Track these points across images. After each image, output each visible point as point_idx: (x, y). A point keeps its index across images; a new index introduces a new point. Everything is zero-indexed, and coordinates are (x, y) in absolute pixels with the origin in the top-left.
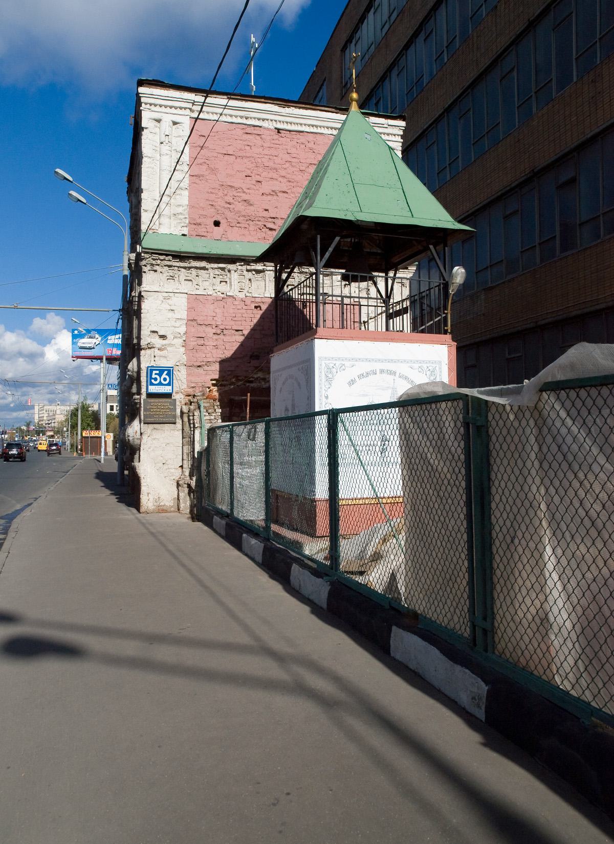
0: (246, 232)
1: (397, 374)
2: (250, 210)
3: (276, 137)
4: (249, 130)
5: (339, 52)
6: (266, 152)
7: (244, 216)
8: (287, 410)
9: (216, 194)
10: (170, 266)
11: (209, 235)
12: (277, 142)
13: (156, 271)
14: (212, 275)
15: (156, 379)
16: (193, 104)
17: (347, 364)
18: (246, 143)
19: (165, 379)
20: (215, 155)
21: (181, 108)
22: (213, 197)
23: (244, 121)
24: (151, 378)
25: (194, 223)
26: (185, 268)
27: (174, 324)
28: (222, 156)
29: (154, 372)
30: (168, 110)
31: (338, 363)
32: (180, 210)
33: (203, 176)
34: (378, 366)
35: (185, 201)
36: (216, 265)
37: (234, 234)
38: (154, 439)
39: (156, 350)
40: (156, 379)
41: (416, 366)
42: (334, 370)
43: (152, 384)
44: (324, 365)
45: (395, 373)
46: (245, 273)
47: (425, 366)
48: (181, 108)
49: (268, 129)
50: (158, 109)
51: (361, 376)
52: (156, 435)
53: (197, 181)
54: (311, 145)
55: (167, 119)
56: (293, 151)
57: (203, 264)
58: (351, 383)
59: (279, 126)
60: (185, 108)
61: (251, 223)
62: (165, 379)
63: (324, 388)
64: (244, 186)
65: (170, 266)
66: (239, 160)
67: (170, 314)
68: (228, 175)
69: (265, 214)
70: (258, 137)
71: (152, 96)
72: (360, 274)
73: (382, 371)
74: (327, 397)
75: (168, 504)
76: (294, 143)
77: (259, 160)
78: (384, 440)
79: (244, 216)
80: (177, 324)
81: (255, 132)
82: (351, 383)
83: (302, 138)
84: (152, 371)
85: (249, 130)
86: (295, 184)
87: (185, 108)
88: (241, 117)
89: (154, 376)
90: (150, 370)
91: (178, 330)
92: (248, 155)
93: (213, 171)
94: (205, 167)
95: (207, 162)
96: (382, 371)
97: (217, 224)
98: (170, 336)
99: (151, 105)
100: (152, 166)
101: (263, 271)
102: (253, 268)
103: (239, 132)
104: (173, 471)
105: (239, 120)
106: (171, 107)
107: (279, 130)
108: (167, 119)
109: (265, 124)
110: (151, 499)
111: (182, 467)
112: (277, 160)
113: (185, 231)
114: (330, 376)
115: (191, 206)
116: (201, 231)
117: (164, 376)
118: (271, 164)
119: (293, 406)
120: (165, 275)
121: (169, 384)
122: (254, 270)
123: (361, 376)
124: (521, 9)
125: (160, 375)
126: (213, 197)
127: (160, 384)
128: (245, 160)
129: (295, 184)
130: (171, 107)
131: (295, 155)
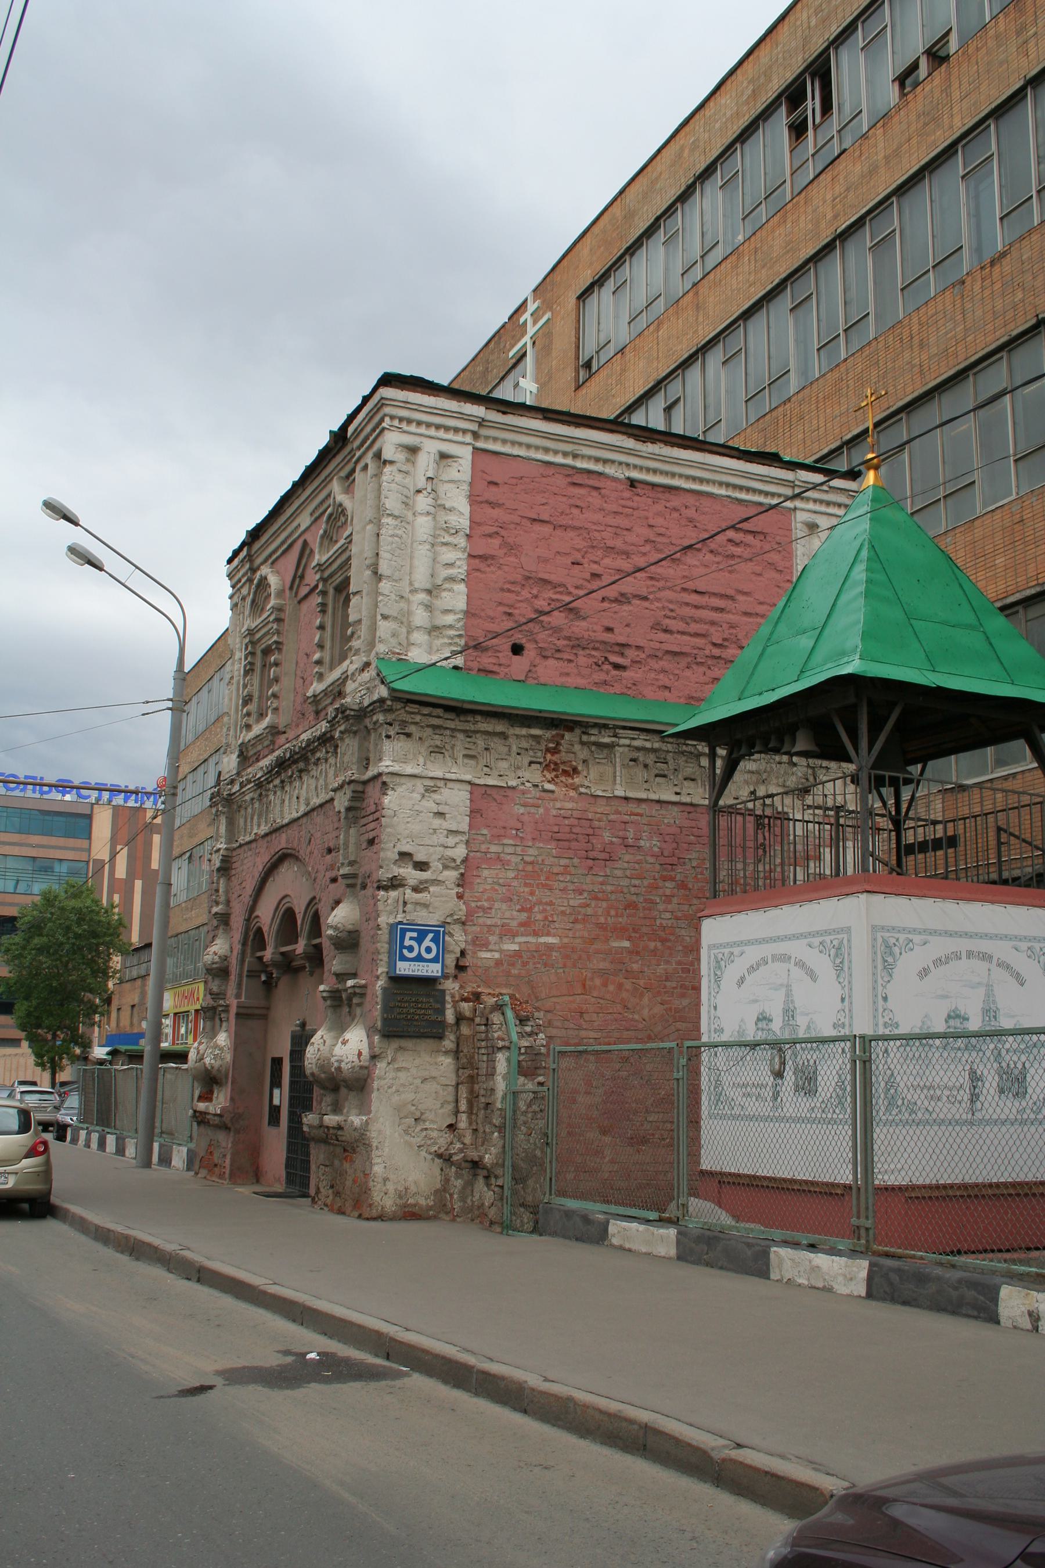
0: (570, 668)
1: (995, 960)
2: (580, 628)
3: (627, 494)
4: (578, 479)
5: (572, 300)
6: (611, 520)
7: (569, 638)
8: (763, 1018)
9: (518, 593)
10: (435, 727)
11: (502, 670)
12: (629, 503)
13: (408, 735)
14: (514, 748)
15: (411, 949)
16: (480, 425)
17: (917, 939)
18: (572, 501)
19: (428, 950)
20: (518, 520)
21: (456, 430)
22: (509, 598)
23: (569, 461)
24: (402, 947)
25: (474, 646)
26: (464, 731)
27: (442, 840)
28: (528, 523)
29: (409, 934)
30: (432, 432)
31: (902, 937)
32: (450, 619)
33: (493, 557)
34: (964, 945)
35: (461, 604)
36: (524, 731)
37: (549, 669)
38: (399, 1069)
39: (408, 891)
40: (411, 949)
41: (1024, 946)
42: (896, 950)
43: (403, 958)
44: (880, 940)
45: (991, 957)
46: (577, 747)
47: (828, 939)
48: (456, 430)
49: (615, 479)
50: (413, 428)
51: (938, 962)
52: (405, 1060)
53: (482, 566)
54: (691, 513)
55: (430, 448)
56: (659, 521)
57: (500, 727)
58: (924, 973)
59: (635, 475)
60: (465, 431)
61: (581, 652)
62: (428, 950)
63: (880, 981)
64: (570, 583)
65: (435, 727)
66: (559, 532)
67: (437, 822)
68: (542, 560)
69: (608, 637)
70: (595, 493)
71: (406, 404)
72: (887, 774)
73: (970, 954)
74: (885, 999)
75: (423, 1202)
76: (659, 507)
77: (596, 534)
78: (975, 1078)
79: (569, 638)
80: (451, 841)
81: (591, 482)
82: (924, 973)
83: (676, 501)
84: (404, 932)
85: (578, 479)
86: (661, 584)
87: (465, 431)
88: (565, 454)
89: (407, 942)
90: (397, 931)
91: (449, 853)
92: (577, 524)
93: (511, 548)
94: (496, 542)
95: (503, 532)
96: (970, 954)
97: (517, 650)
98: (436, 865)
99: (401, 419)
100: (399, 532)
101: (610, 746)
102: (593, 739)
103: (561, 481)
104: (435, 1134)
105: (559, 459)
106: (438, 427)
107: (632, 483)
108: (430, 448)
109: (609, 470)
110: (391, 1191)
111: (451, 1127)
112: (631, 538)
113: (459, 661)
114: (890, 959)
115: (469, 614)
116: (487, 660)
117: (427, 942)
118: (618, 543)
119: (789, 1013)
120: (427, 744)
121: (435, 960)
122: (595, 744)
123: (938, 962)
124: (1020, 295)
125: (420, 940)
126: (509, 598)
127: (419, 958)
128: (571, 534)
129: (661, 584)
130: (438, 427)
131: (662, 530)
